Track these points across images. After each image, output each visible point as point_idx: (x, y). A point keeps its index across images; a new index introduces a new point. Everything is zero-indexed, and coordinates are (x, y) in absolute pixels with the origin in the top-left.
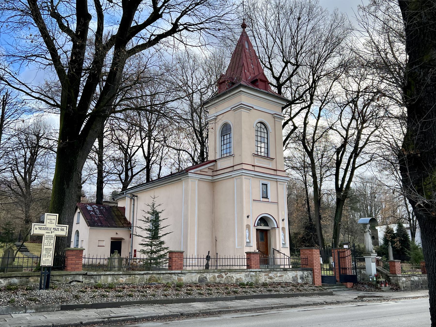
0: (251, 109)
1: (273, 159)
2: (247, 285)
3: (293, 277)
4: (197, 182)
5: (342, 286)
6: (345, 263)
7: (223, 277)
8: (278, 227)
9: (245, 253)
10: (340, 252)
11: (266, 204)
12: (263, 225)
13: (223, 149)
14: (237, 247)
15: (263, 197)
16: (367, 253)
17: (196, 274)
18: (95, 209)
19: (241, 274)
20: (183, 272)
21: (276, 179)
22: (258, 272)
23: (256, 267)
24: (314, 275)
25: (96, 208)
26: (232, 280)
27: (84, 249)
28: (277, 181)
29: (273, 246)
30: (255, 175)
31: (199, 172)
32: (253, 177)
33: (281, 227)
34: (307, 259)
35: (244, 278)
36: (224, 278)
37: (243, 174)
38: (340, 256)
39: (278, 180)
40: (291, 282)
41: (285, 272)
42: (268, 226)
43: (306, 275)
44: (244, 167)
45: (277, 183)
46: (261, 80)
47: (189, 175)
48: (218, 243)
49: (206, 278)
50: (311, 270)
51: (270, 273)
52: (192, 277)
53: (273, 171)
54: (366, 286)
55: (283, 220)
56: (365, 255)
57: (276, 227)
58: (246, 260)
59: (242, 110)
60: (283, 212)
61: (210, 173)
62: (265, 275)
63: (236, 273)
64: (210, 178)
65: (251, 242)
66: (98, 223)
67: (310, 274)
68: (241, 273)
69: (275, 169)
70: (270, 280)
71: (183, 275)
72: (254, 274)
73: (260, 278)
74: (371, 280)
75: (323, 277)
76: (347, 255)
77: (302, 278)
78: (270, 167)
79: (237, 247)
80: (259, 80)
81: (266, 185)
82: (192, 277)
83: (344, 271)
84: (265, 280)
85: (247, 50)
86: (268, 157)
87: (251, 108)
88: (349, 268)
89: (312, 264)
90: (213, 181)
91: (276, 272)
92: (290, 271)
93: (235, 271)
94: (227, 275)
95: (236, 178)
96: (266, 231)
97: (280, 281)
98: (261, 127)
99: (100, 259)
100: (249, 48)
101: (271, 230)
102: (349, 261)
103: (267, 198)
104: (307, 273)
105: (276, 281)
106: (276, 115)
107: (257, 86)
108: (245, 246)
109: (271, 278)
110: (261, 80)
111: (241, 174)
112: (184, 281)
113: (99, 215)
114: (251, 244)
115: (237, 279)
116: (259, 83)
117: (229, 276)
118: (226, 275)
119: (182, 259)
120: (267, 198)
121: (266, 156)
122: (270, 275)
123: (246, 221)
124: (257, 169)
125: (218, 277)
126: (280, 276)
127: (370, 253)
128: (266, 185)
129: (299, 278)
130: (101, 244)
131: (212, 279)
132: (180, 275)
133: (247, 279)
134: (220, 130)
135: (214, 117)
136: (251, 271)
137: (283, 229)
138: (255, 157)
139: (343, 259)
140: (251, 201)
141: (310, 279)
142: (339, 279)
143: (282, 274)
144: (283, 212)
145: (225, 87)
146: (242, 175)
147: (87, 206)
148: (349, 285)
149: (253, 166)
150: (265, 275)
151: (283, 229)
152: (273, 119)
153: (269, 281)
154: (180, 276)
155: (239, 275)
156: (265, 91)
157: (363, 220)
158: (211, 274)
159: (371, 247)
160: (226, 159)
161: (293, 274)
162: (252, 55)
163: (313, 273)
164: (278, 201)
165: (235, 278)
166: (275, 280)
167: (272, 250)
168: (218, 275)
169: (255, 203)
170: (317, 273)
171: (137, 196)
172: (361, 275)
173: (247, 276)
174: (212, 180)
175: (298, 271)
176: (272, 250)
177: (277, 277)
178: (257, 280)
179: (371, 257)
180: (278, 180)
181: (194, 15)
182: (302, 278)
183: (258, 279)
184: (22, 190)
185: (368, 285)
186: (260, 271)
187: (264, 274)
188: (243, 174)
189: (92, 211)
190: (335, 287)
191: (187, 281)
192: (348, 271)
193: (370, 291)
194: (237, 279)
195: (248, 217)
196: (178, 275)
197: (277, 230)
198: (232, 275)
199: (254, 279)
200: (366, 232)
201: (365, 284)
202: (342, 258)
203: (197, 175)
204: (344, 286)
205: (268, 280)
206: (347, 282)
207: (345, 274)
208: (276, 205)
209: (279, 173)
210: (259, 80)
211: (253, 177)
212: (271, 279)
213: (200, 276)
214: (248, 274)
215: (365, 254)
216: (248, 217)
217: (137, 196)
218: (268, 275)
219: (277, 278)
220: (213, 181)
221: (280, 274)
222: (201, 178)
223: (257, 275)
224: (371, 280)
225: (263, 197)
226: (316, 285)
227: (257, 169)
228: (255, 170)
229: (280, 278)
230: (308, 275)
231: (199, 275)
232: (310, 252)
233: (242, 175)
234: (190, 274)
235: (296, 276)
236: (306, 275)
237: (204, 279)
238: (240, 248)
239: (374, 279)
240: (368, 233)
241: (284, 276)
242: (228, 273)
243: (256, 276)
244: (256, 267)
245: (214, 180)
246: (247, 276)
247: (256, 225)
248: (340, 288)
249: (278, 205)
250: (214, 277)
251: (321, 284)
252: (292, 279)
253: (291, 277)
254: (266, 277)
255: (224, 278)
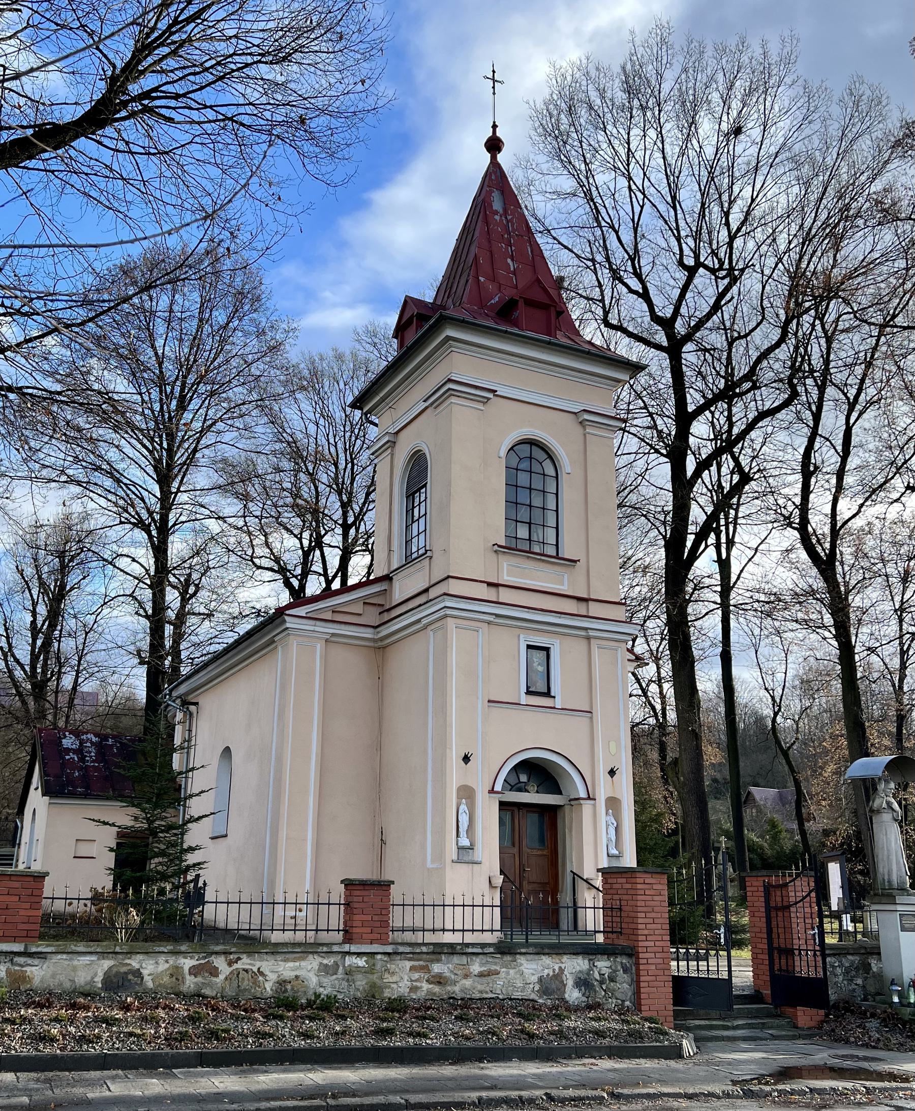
0: (489, 399)
1: (575, 561)
2: (310, 1004)
3: (540, 980)
4: (319, 647)
5: (776, 1022)
6: (788, 929)
7: (214, 972)
8: (589, 798)
9: (342, 882)
10: (773, 886)
11: (540, 716)
12: (533, 787)
13: (422, 536)
14: (429, 865)
15: (529, 692)
16: (883, 895)
17: (94, 958)
18: (89, 744)
19: (303, 963)
20: (34, 950)
21: (586, 629)
22: (379, 957)
23: (371, 936)
24: (638, 975)
25: (92, 742)
26: (256, 983)
27: (393, 882)
28: (588, 638)
29: (571, 865)
30: (497, 616)
31: (328, 616)
32: (489, 623)
33: (601, 796)
34: (620, 909)
35: (314, 980)
36: (222, 977)
37: (449, 612)
38: (773, 904)
39: (591, 633)
40: (533, 996)
41: (508, 958)
42: (560, 793)
43: (606, 972)
44: (455, 587)
45: (589, 644)
46: (530, 303)
47: (288, 625)
48: (388, 850)
49: (138, 973)
50: (630, 955)
51: (438, 961)
52: (75, 969)
53: (574, 602)
54: (873, 1024)
55: (612, 773)
56: (876, 899)
57: (583, 794)
58: (497, 911)
59: (453, 400)
60: (613, 745)
61: (371, 617)
62: (412, 969)
63: (279, 957)
64: (368, 633)
65: (479, 846)
66: (75, 787)
67: (625, 971)
68: (304, 959)
69: (585, 596)
70: (436, 989)
71: (36, 962)
72: (361, 962)
73: (388, 978)
74: (896, 999)
75: (680, 985)
76: (792, 899)
77: (583, 983)
78: (564, 589)
79: (429, 865)
80: (521, 304)
81: (547, 650)
82: (75, 969)
83: (783, 961)
84: (414, 989)
85: (497, 217)
86: (557, 557)
87: (490, 395)
88: (800, 950)
89: (634, 932)
90: (380, 644)
91: (464, 959)
92: (529, 957)
93: (276, 950)
94: (235, 966)
95: (433, 627)
96: (552, 811)
97: (481, 992)
98: (531, 458)
99: (285, 903)
100: (505, 210)
101: (567, 808)
102: (809, 921)
103: (548, 694)
104: (608, 964)
105: (462, 991)
106: (587, 416)
107: (515, 324)
108: (448, 861)
109: (439, 980)
110: (530, 303)
111: (442, 613)
112: (36, 982)
113: (93, 761)
114: (478, 854)
115: (282, 983)
116: (521, 311)
117: (246, 971)
118: (230, 964)
119: (384, 910)
120: (548, 694)
121: (551, 551)
122: (437, 968)
123: (456, 775)
124: (505, 595)
125: (194, 971)
126: (481, 975)
127: (895, 892)
128: (547, 650)
129: (570, 983)
130: (84, 850)
131: (166, 979)
132: (21, 960)
133: (326, 981)
134: (403, 478)
135: (386, 439)
136: (349, 953)
137: (613, 803)
138: (501, 556)
139: (780, 914)
140: (481, 704)
141: (623, 985)
142: (769, 992)
143: (493, 967)
144: (613, 745)
145: (411, 336)
146: (446, 616)
147: (65, 737)
148: (805, 1016)
149: (490, 584)
150: (412, 969)
151: (613, 803)
152: (579, 429)
153: (429, 992)
154: (22, 966)
155: (291, 964)
156: (546, 338)
157: (863, 765)
158: (161, 959)
159: (899, 870)
160: (412, 569)
161: (544, 968)
162: (206, 157)
163: (637, 964)
164: (591, 707)
165: (272, 977)
166: (457, 989)
167: (569, 878)
168: (194, 962)
169: (496, 711)
170: (653, 967)
171: (196, 704)
172: (870, 981)
173: (326, 970)
174: (374, 640)
175: (565, 958)
176: (569, 878)
177: (466, 976)
178: (373, 985)
179: (899, 908)
180: (591, 633)
181: (774, 240)
182: (583, 983)
183: (378, 982)
184: (24, 703)
185: (884, 1020)
186: (389, 954)
187: (408, 964)
188: (449, 612)
189: (75, 751)
190: (740, 1022)
191: (52, 983)
192: (797, 963)
193: (881, 1045)
194: (282, 983)
195: (466, 759)
196: (12, 960)
197: (587, 807)
198: (258, 964)
199: (361, 982)
200: (878, 812)
201: (873, 1015)
202: (777, 909)
203: (318, 623)
204: (783, 1022)
205: (425, 986)
206: (794, 1006)
207: (787, 971)
208: (583, 721)
209: (595, 609)
210: (521, 304)
211: (489, 623)
212: (439, 983)
213: (110, 968)
214: (336, 964)
215: (875, 895)
216: (466, 759)
217: (196, 704)
218: (426, 969)
219: (468, 983)
220: (380, 644)
221: (481, 965)
222: (333, 635)
223: (378, 967)
224: (896, 999)
225: (529, 692)
226: (644, 1014)
227: (505, 595)
228: (590, 615)
229: (485, 980)
230: (615, 971)
231: (107, 964)
232: (629, 886)
233: (446, 616)
234: (64, 956)
235: (558, 976)
236: (606, 972)
237: (130, 977)
238: (437, 869)
239: (908, 997)
240: (887, 817)
241: (502, 975)
242: (244, 956)
243: (371, 970)
244: (371, 936)
245: (382, 639)
246: (326, 970)
247: (498, 787)
248: (763, 1026)
249: (591, 718)
250: (176, 973)
251: (671, 1007)
252: (537, 988)
253: (535, 979)
254: (416, 976)
255: (222, 977)
